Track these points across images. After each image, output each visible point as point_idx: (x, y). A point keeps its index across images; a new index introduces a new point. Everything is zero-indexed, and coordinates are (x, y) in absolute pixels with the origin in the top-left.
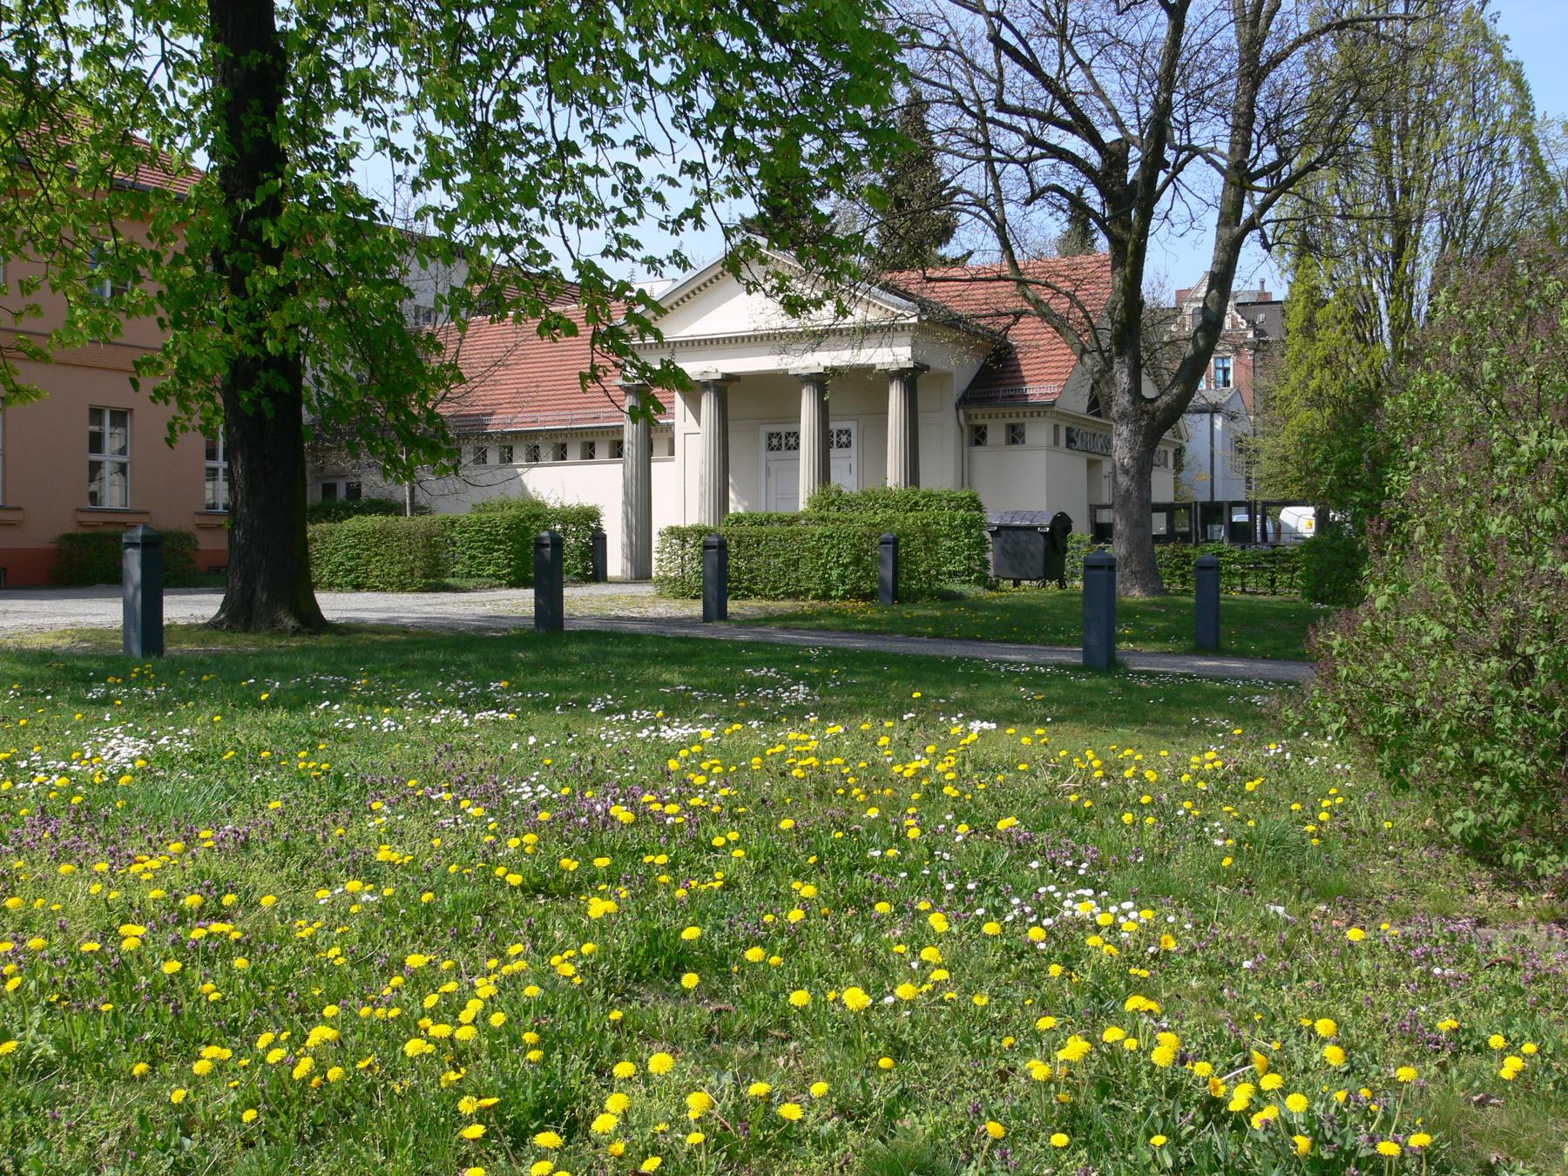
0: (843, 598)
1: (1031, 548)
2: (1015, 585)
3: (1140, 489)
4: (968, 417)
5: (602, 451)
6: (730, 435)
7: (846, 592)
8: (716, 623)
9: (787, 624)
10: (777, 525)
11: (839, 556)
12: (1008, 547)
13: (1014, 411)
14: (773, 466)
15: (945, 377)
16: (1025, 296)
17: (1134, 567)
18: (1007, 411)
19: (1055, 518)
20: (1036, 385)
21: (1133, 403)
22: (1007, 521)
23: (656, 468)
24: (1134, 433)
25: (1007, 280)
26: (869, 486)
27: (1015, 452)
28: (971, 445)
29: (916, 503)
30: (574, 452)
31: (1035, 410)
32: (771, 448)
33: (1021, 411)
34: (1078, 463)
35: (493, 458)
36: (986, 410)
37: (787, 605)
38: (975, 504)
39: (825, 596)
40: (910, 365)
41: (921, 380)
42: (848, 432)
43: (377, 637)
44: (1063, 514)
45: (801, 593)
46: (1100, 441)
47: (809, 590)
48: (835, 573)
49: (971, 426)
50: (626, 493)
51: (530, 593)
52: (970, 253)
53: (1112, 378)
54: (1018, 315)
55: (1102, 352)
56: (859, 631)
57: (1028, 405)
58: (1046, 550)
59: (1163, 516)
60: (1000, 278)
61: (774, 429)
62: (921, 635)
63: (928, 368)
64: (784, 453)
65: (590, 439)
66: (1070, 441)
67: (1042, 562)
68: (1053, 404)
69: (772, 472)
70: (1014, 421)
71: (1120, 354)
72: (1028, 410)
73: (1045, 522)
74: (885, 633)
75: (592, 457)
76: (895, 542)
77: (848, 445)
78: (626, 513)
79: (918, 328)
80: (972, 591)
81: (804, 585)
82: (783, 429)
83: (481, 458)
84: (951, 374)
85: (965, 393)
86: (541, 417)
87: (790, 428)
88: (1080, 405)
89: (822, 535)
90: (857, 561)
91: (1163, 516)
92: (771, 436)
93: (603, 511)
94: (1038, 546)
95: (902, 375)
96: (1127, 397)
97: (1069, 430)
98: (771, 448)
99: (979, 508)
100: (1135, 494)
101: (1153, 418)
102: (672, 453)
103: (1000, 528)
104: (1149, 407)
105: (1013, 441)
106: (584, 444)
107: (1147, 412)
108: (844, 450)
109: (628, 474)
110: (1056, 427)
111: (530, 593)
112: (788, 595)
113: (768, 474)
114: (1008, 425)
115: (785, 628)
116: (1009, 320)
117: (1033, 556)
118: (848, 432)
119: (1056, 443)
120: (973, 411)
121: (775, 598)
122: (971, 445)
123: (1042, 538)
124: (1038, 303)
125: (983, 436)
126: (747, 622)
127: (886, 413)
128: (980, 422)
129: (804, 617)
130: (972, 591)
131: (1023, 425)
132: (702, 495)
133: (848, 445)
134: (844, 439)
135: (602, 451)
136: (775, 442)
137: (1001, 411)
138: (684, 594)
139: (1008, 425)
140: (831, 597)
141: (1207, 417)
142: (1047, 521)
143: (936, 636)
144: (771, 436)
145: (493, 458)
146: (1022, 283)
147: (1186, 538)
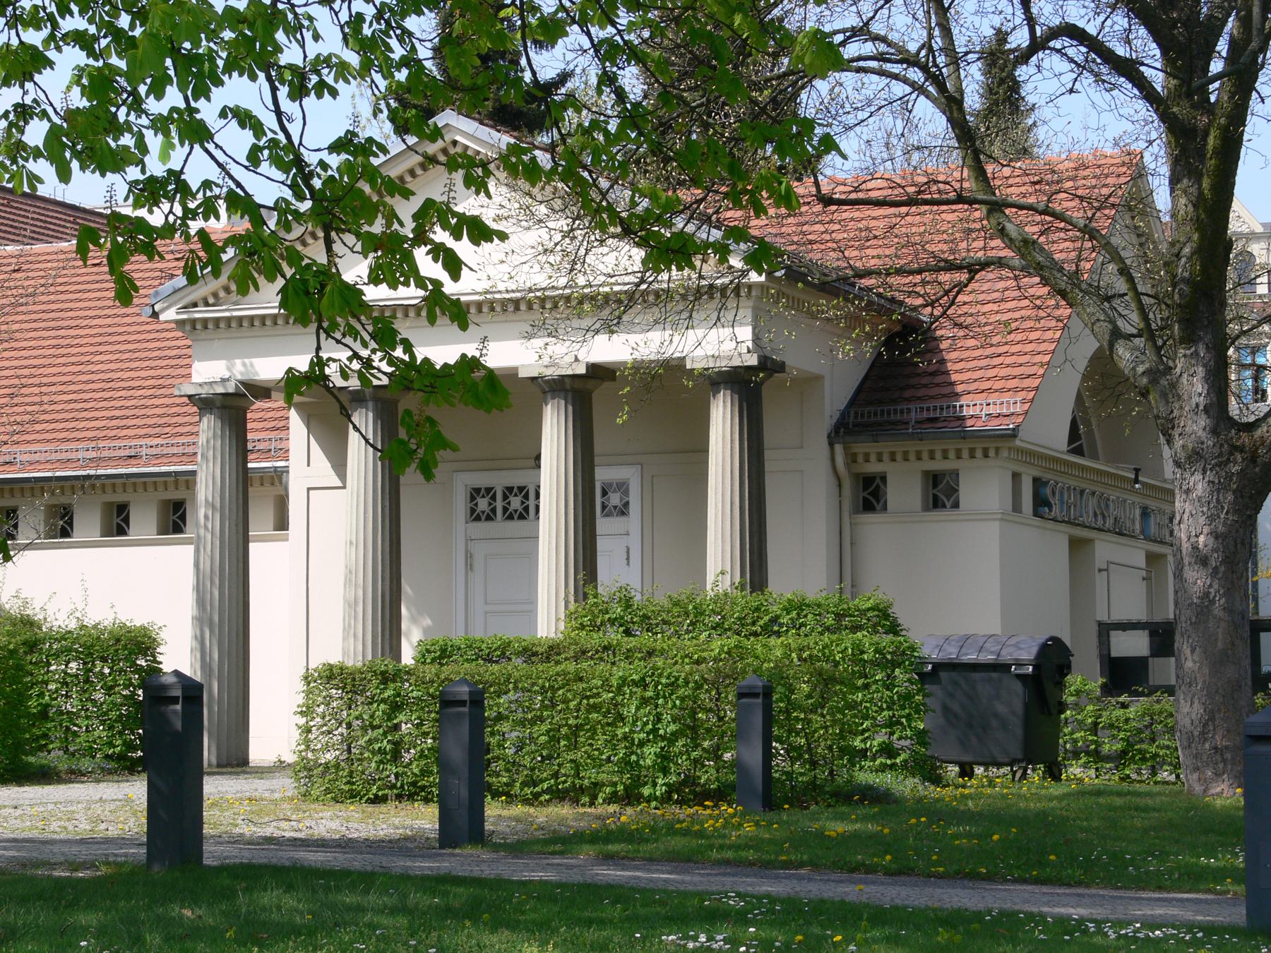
0: (666, 799)
1: (1001, 708)
2: (963, 774)
4: (852, 459)
5: (144, 520)
6: (403, 490)
7: (671, 789)
8: (468, 850)
9: (613, 848)
10: (518, 661)
11: (658, 719)
12: (956, 707)
13: (938, 447)
14: (480, 550)
15: (811, 381)
16: (1002, 232)
18: (924, 447)
19: (1044, 648)
20: (979, 399)
22: (951, 653)
25: (971, 202)
26: (681, 591)
27: (941, 525)
28: (856, 511)
29: (775, 620)
30: (88, 523)
31: (979, 447)
32: (475, 516)
33: (951, 446)
34: (1055, 542)
36: (885, 447)
37: (562, 814)
38: (886, 620)
39: (630, 797)
42: (623, 487)
43: (709, 871)
44: (1056, 641)
45: (582, 790)
46: (1092, 503)
47: (597, 786)
48: (650, 752)
49: (856, 476)
50: (201, 602)
51: (136, 790)
52: (844, 157)
53: (1173, 385)
54: (974, 268)
55: (1152, 337)
56: (751, 864)
57: (965, 435)
58: (1027, 707)
60: (960, 199)
61: (482, 480)
62: (870, 870)
63: (781, 367)
64: (500, 526)
65: (120, 498)
66: (1041, 503)
67: (1019, 731)
68: (1014, 434)
69: (478, 562)
70: (938, 465)
71: (1188, 339)
72: (965, 447)
73: (1025, 652)
74: (787, 865)
75: (121, 531)
76: (767, 693)
77: (623, 511)
78: (201, 640)
80: (907, 786)
81: (590, 775)
82: (499, 481)
85: (844, 414)
86: (145, 446)
87: (515, 479)
88: (1055, 437)
89: (624, 681)
90: (692, 730)
92: (475, 493)
93: (163, 635)
97: (1036, 480)
98: (475, 516)
99: (894, 629)
102: (282, 523)
103: (938, 666)
105: (935, 503)
106: (108, 506)
108: (516, 525)
109: (206, 564)
110: (1016, 476)
111: (136, 790)
112: (559, 795)
113: (469, 566)
114: (926, 474)
115: (608, 858)
116: (963, 276)
118: (623, 487)
119: (1017, 507)
120: (860, 448)
121: (533, 800)
122: (856, 511)
123: (1018, 687)
124: (1026, 246)
125: (953, 491)
126: (518, 848)
127: (705, 450)
128: (873, 467)
129: (624, 835)
130: (907, 786)
131: (955, 474)
132: (351, 605)
133: (623, 511)
134: (615, 499)
135: (144, 520)
136: (483, 504)
137: (912, 447)
138: (353, 795)
139: (926, 474)
140: (639, 798)
142: (1028, 653)
143: (898, 873)
144: (475, 493)
146: (996, 207)
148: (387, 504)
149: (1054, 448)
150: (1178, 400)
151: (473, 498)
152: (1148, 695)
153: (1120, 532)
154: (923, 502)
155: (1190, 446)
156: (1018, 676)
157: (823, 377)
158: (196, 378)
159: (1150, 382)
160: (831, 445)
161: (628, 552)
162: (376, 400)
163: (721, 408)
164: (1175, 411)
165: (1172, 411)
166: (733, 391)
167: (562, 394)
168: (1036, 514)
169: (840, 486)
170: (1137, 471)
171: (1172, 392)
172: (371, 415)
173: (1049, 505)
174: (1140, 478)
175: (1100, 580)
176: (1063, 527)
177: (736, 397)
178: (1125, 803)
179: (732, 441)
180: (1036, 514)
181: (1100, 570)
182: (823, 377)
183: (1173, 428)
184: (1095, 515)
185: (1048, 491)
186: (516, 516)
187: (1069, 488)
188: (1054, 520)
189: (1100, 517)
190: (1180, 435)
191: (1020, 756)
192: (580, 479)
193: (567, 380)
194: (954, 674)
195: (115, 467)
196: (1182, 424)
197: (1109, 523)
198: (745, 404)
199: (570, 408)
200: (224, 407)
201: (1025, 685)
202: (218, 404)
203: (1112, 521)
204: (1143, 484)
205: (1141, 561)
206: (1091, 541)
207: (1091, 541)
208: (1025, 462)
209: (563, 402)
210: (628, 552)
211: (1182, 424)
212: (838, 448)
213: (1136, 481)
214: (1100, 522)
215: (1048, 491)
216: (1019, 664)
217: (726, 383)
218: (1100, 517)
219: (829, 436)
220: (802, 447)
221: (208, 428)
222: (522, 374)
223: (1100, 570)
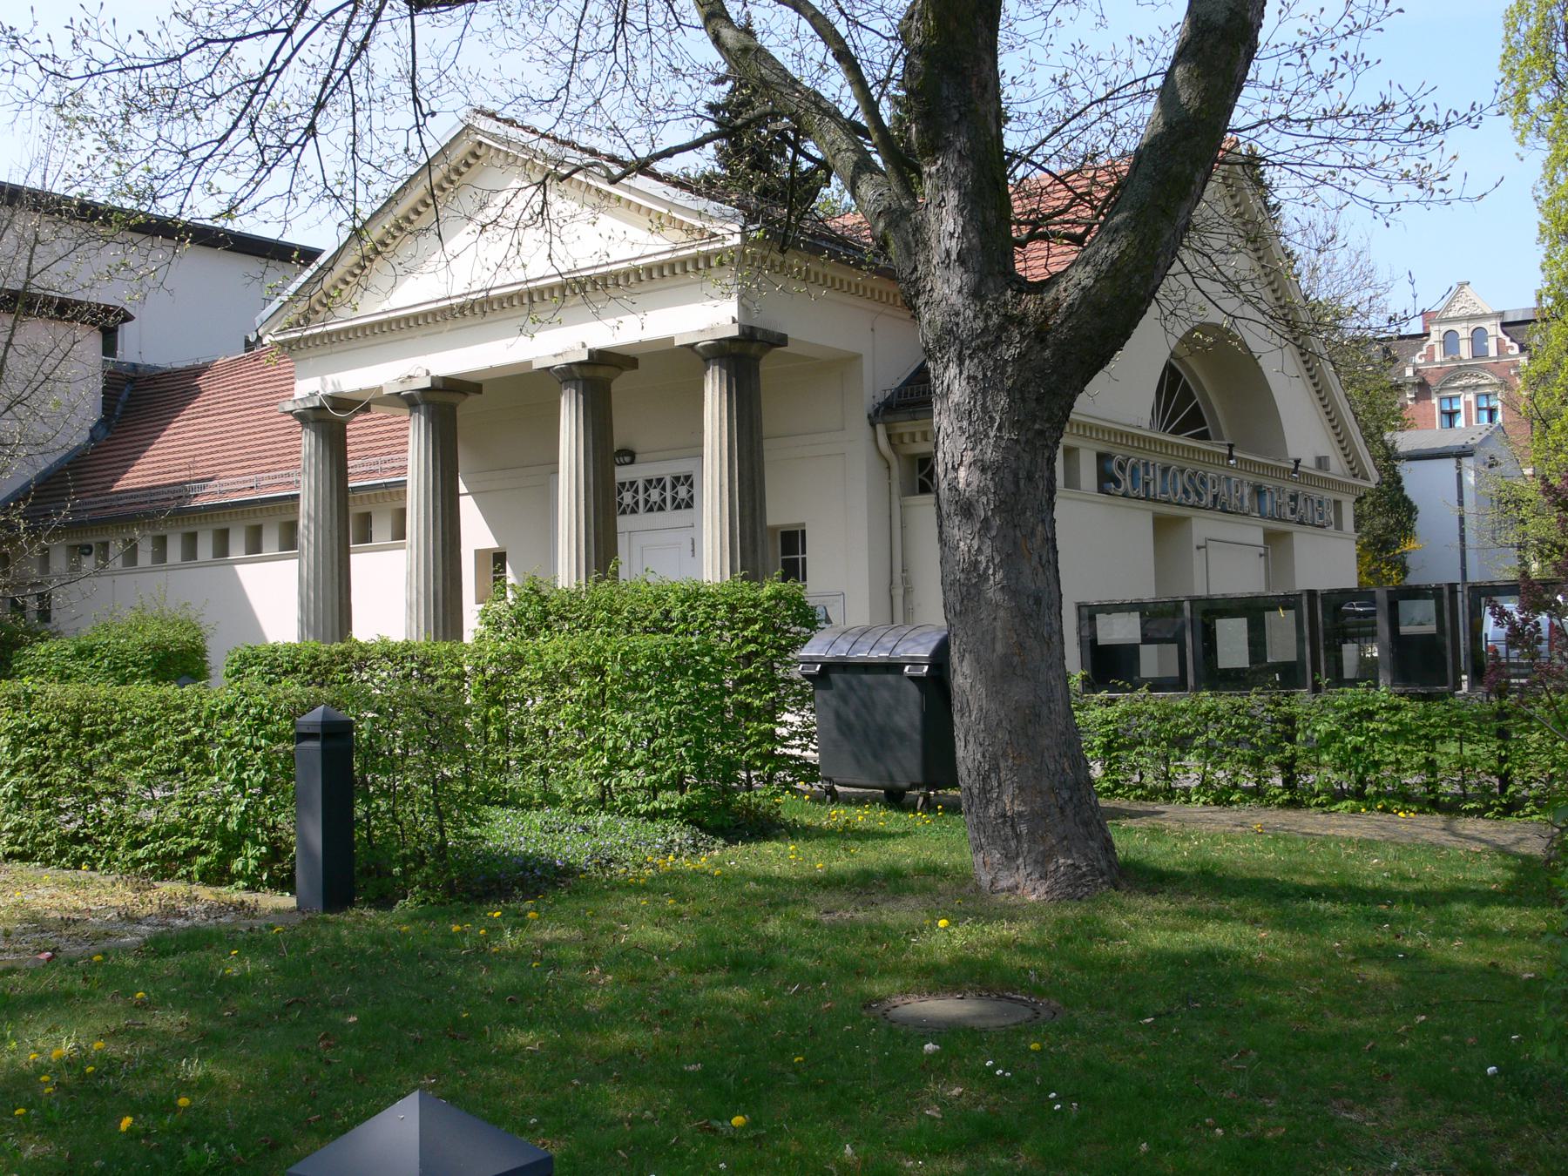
3: (1010, 560)
15: (842, 365)
17: (1011, 803)
21: (976, 294)
23: (361, 563)
24: (982, 386)
35: (205, 548)
40: (734, 331)
41: (768, 365)
53: (918, 229)
59: (1242, 623)
79: (738, 259)
83: (160, 555)
84: (857, 358)
91: (1242, 623)
94: (908, 714)
95: (723, 352)
96: (957, 278)
97: (1102, 458)
100: (996, 577)
101: (1041, 334)
102: (400, 533)
104: (1030, 303)
107: (1021, 321)
108: (683, 512)
117: (902, 736)
123: (913, 690)
141: (1453, 461)
145: (205, 548)
147: (1290, 676)
148: (439, 504)
149: (1108, 418)
150: (923, 249)
151: (692, 498)
152: (1131, 691)
153: (1220, 506)
154: (761, 457)
155: (939, 320)
156: (912, 678)
157: (860, 356)
158: (297, 396)
159: (887, 226)
160: (873, 425)
161: (693, 544)
162: (427, 403)
163: (710, 385)
164: (920, 268)
165: (915, 269)
166: (721, 366)
167: (573, 384)
168: (1101, 490)
169: (889, 468)
170: (1231, 447)
171: (917, 240)
172: (423, 418)
173: (1117, 483)
174: (1234, 454)
175: (1198, 558)
176: (1142, 504)
177: (724, 371)
178: (1010, 858)
179: (720, 419)
180: (1101, 490)
181: (1198, 548)
182: (860, 356)
183: (917, 295)
184: (1185, 491)
185: (1114, 466)
186: (655, 508)
187: (1146, 465)
188: (1124, 495)
189: (1192, 495)
190: (927, 303)
191: (918, 778)
192: (591, 465)
193: (574, 368)
194: (848, 676)
195: (361, 480)
196: (928, 288)
197: (1207, 499)
198: (734, 380)
199: (581, 397)
200: (317, 421)
201: (921, 690)
202: (312, 419)
203: (1210, 498)
204: (1237, 459)
205: (1257, 537)
206: (1186, 519)
207: (1186, 519)
208: (1139, 448)
209: (574, 391)
210: (693, 544)
211: (928, 288)
212: (880, 428)
213: (1231, 457)
214: (1193, 498)
215: (1114, 466)
216: (915, 663)
217: (714, 358)
218: (1192, 495)
219: (869, 416)
220: (843, 429)
221: (307, 441)
222: (536, 366)
223: (1198, 548)
